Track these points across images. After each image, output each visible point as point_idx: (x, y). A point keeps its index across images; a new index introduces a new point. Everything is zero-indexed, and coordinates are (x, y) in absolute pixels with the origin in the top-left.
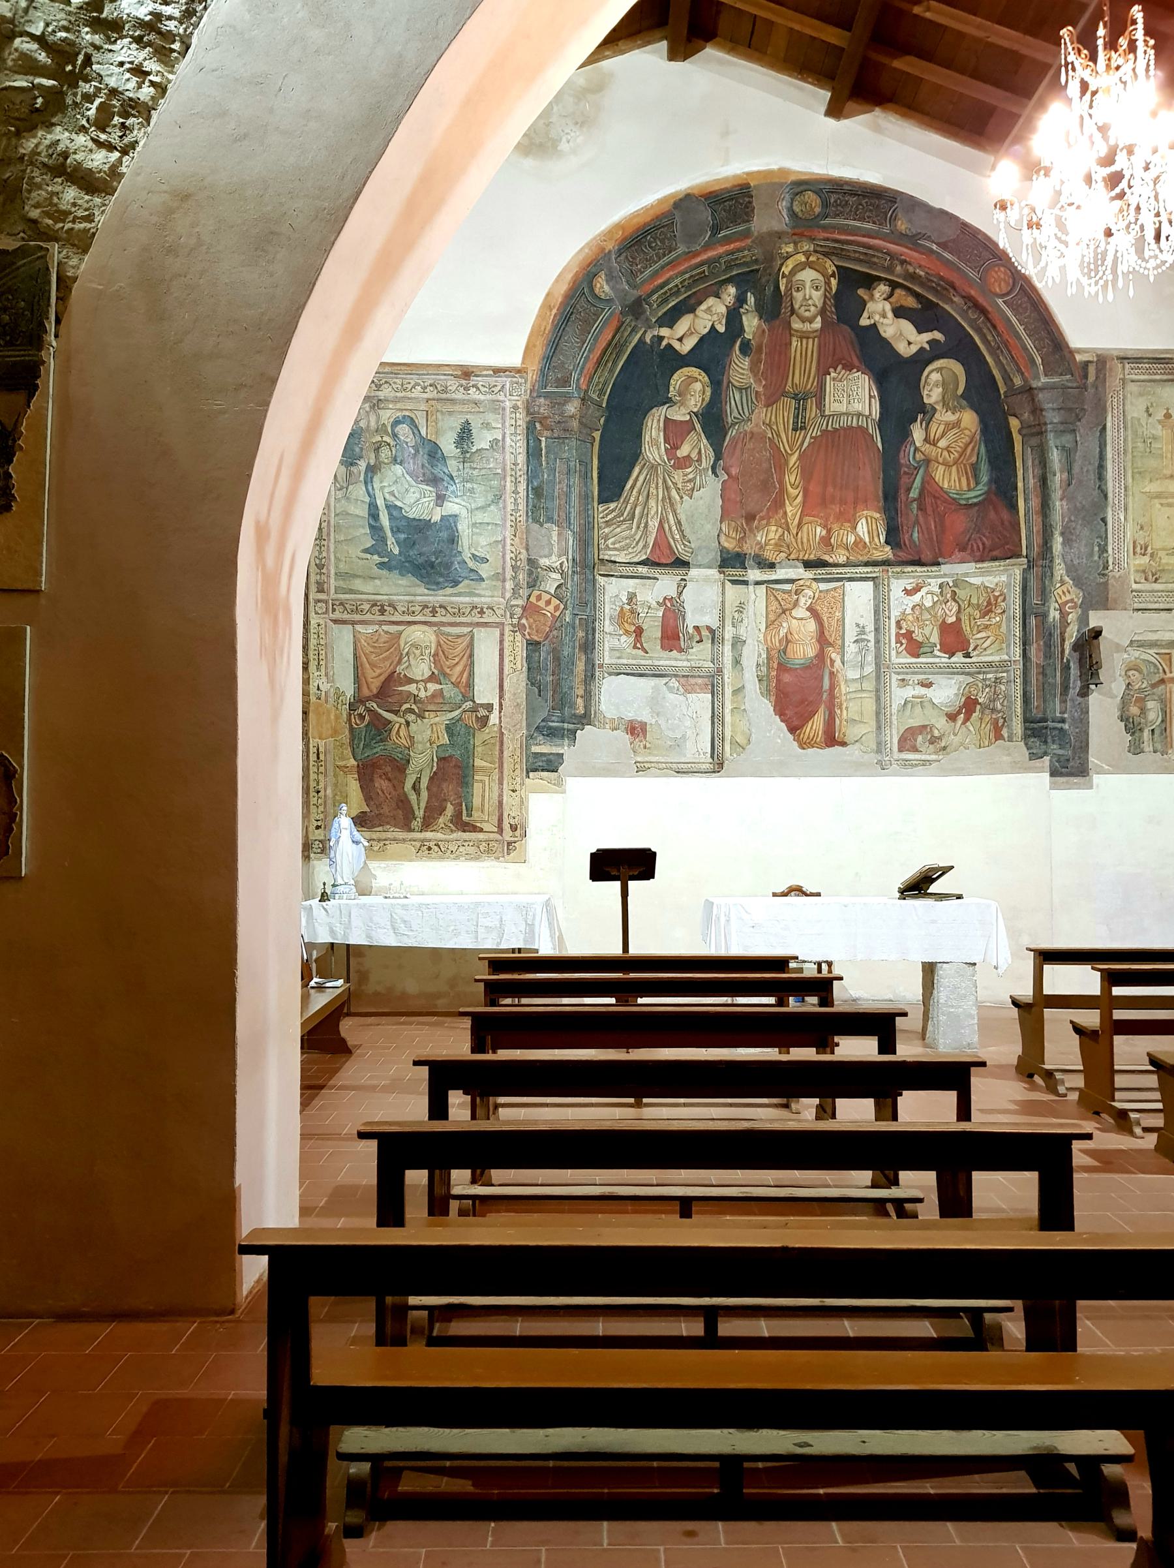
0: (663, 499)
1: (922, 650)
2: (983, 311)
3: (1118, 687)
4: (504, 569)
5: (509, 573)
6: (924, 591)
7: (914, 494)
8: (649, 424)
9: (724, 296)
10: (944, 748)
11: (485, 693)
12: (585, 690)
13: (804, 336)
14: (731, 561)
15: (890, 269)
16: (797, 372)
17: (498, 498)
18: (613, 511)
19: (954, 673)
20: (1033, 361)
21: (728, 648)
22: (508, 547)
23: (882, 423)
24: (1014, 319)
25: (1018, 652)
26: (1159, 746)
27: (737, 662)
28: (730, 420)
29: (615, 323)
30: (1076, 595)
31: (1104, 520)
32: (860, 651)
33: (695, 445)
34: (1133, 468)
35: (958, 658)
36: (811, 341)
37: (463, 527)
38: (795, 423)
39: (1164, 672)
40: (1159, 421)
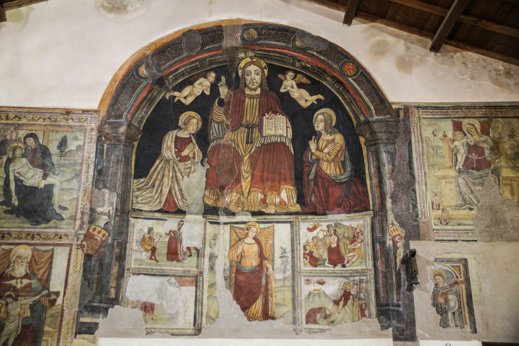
0: (172, 177)
1: (318, 263)
2: (341, 84)
3: (430, 286)
4: (76, 214)
5: (79, 215)
6: (318, 229)
7: (311, 177)
8: (167, 139)
9: (209, 77)
10: (333, 322)
11: (56, 284)
12: (117, 284)
13: (251, 97)
14: (210, 211)
15: (293, 64)
16: (248, 115)
17: (78, 175)
18: (142, 183)
19: (336, 276)
20: (369, 109)
21: (207, 260)
22: (80, 202)
23: (293, 141)
24: (358, 88)
25: (370, 265)
26: (458, 323)
27: (212, 268)
28: (212, 138)
29: (148, 89)
30: (401, 232)
31: (414, 191)
32: (283, 263)
33: (192, 150)
34: (428, 163)
35: (339, 268)
36: (255, 100)
37: (56, 191)
38: (247, 140)
39: (457, 277)
40: (441, 139)
